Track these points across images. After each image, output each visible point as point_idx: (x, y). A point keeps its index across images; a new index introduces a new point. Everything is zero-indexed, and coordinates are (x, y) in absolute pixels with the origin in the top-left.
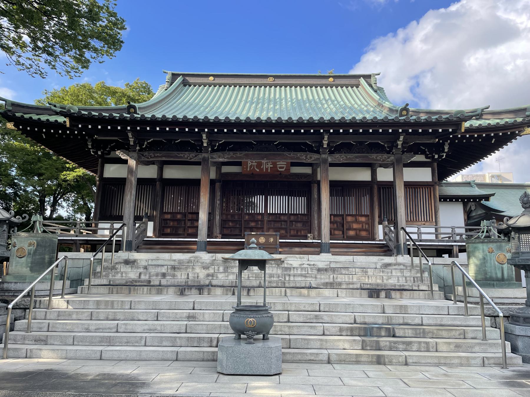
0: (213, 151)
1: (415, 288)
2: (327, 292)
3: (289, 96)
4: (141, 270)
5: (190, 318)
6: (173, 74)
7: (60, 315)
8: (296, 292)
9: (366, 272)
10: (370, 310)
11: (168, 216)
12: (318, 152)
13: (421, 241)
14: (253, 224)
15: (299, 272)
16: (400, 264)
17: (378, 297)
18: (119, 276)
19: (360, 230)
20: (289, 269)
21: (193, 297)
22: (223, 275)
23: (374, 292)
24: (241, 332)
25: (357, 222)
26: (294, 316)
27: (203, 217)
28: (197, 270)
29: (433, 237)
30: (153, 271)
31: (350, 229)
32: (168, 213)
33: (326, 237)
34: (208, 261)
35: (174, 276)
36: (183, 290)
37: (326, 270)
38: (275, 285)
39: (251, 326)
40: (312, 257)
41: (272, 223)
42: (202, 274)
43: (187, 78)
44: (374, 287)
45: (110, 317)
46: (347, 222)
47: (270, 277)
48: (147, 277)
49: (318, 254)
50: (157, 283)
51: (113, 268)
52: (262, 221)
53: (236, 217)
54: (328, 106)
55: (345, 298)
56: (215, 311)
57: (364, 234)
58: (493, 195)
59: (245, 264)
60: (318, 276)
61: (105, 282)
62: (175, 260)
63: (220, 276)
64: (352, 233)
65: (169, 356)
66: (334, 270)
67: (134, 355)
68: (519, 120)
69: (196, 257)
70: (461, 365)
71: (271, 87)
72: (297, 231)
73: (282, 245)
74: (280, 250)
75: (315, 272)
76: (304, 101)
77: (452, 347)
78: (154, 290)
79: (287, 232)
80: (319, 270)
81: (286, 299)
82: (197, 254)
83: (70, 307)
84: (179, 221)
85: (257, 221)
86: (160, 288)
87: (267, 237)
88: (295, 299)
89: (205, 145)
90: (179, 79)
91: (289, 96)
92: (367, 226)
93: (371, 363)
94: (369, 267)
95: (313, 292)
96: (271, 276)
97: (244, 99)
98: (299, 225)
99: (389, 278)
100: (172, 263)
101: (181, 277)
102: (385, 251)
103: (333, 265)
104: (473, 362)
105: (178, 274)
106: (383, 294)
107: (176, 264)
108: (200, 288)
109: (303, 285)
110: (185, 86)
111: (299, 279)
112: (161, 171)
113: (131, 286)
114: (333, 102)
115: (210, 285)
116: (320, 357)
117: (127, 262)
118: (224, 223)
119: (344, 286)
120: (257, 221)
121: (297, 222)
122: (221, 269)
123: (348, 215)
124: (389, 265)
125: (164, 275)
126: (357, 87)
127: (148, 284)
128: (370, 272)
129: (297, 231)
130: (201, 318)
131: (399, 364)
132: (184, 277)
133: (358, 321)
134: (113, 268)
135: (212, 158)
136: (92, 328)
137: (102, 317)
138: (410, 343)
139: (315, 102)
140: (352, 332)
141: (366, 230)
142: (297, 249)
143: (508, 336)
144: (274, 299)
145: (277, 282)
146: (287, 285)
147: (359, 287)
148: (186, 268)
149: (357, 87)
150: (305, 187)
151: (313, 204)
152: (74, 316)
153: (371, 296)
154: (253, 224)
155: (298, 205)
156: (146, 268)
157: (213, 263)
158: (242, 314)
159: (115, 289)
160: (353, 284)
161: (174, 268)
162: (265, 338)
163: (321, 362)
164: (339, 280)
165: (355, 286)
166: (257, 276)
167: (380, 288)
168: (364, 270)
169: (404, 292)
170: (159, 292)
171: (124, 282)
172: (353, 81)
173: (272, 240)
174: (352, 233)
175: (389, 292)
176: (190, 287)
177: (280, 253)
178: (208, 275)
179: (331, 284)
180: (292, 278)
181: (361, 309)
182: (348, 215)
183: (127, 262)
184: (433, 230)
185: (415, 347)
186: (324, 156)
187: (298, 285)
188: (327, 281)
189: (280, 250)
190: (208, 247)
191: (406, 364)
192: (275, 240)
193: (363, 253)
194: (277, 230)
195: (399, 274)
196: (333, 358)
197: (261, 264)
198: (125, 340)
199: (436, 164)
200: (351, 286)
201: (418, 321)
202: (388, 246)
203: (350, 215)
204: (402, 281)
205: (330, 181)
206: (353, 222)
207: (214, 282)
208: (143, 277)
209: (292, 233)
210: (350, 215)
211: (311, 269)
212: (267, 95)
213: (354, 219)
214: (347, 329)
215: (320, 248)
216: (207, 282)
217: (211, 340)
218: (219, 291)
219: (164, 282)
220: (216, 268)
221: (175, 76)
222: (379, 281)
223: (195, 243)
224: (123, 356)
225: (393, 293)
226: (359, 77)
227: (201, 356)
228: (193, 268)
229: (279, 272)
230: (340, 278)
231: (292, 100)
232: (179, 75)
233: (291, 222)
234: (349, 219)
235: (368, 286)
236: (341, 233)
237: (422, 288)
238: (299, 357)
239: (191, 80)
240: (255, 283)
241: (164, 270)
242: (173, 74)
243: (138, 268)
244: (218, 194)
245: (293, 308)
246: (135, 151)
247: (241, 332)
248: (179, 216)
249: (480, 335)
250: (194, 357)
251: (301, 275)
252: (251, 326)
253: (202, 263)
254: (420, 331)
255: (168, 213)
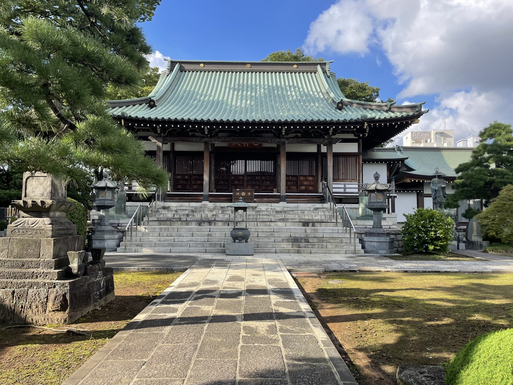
0: (211, 136)
1: (329, 221)
2: (280, 224)
3: (262, 83)
4: (174, 212)
5: (208, 235)
6: (172, 62)
7: (144, 234)
8: (262, 224)
9: (304, 213)
10: (299, 231)
11: (179, 177)
12: (279, 137)
13: (345, 193)
14: (237, 182)
15: (265, 213)
16: (324, 208)
17: (308, 226)
18: (162, 216)
19: (309, 186)
20: (260, 211)
21: (206, 227)
22: (221, 215)
23: (306, 224)
24: (235, 238)
25: (306, 180)
26: (260, 234)
27: (206, 178)
28: (206, 212)
29: (357, 190)
30: (180, 212)
31: (302, 185)
32: (179, 175)
33: (283, 191)
34: (212, 207)
35: (193, 216)
36: (200, 223)
37: (281, 212)
38: (251, 220)
39: (240, 236)
40: (273, 205)
41: (250, 181)
42: (210, 215)
43: (183, 65)
44: (307, 221)
45: (169, 235)
46: (300, 181)
47: (249, 216)
48: (178, 216)
49: (278, 202)
50: (185, 220)
51: (157, 211)
52: (243, 180)
53: (225, 177)
54: (291, 92)
55: (289, 226)
56: (221, 232)
57: (311, 188)
58: (407, 158)
59: (237, 209)
60: (276, 215)
61: (155, 219)
62: (192, 207)
63: (220, 216)
64: (303, 188)
65: (202, 251)
66: (285, 212)
67: (186, 250)
68: (411, 114)
69: (204, 205)
70: (336, 253)
71: (248, 72)
72: (267, 187)
73: (256, 197)
74: (255, 200)
75: (275, 213)
76: (273, 87)
77: (334, 246)
78: (184, 223)
79: (259, 188)
80: (277, 212)
81: (257, 227)
82: (204, 202)
83: (147, 231)
84: (186, 180)
85: (239, 180)
86: (187, 222)
87: (247, 192)
88: (262, 227)
89: (206, 133)
90: (177, 66)
91: (262, 83)
92: (313, 183)
93: (295, 253)
94: (307, 209)
95: (272, 224)
96: (249, 215)
97: (228, 85)
98: (268, 183)
99: (316, 216)
100: (191, 208)
101: (198, 216)
102: (321, 200)
103: (285, 209)
104: (341, 252)
105: (196, 214)
106: (311, 224)
107: (193, 209)
108: (210, 222)
109: (267, 220)
110: (182, 71)
111: (265, 217)
112: (173, 145)
113: (170, 221)
114: (295, 87)
115: (215, 221)
116: (272, 251)
117: (164, 208)
118: (217, 182)
119: (290, 221)
120: (239, 180)
121: (266, 180)
122: (220, 212)
123: (300, 176)
124: (318, 208)
125: (188, 215)
126: (315, 73)
127: (180, 220)
128: (306, 213)
129: (267, 187)
130: (214, 235)
131: (308, 253)
132: (199, 216)
133: (292, 236)
134: (157, 211)
135: (211, 141)
136: (162, 240)
137: (165, 235)
138: (314, 245)
139: (282, 88)
140: (288, 240)
141: (312, 186)
142: (266, 199)
143: (361, 241)
144: (251, 227)
145: (253, 219)
146: (258, 220)
147: (298, 220)
148: (200, 211)
149: (315, 73)
150: (271, 155)
151: (277, 167)
152: (151, 235)
153: (304, 226)
154: (237, 182)
155: (268, 166)
156: (176, 211)
157: (215, 208)
158: (236, 231)
159: (162, 223)
160: (295, 219)
161: (193, 211)
162: (246, 242)
163: (272, 253)
164: (288, 217)
165: (296, 221)
166: (241, 216)
167: (310, 221)
168: (303, 211)
169: (322, 223)
170: (187, 224)
171: (166, 219)
172: (312, 68)
173: (249, 194)
174: (303, 188)
175: (314, 223)
176: (204, 222)
177: (255, 202)
178: (213, 215)
179: (283, 219)
180: (261, 217)
181: (295, 231)
182: (300, 176)
183: (164, 208)
184: (357, 186)
185: (316, 246)
186: (283, 140)
187: (264, 220)
188: (281, 218)
189: (255, 200)
190: (210, 198)
191: (311, 253)
192: (252, 194)
193: (317, 199)
194: (253, 186)
195: (323, 214)
196: (278, 251)
197: (245, 209)
198: (180, 245)
199: (361, 140)
200: (294, 221)
201: (321, 236)
202: (323, 197)
203: (302, 176)
204: (323, 218)
205: (287, 153)
206: (304, 181)
207: (217, 219)
208: (176, 216)
209: (263, 188)
210: (302, 176)
211: (273, 211)
212: (245, 82)
213: (305, 178)
214: (286, 239)
215: (279, 199)
216: (213, 219)
217: (221, 244)
218: (220, 224)
219: (188, 219)
220: (217, 211)
221: (173, 64)
222: (310, 218)
223: (202, 195)
224: (180, 251)
225: (316, 224)
226: (317, 64)
227: (217, 250)
228: (204, 212)
229: (254, 213)
230: (288, 216)
231: (264, 86)
232: (176, 62)
233: (263, 180)
234: (302, 178)
235: (304, 221)
236: (296, 187)
237: (332, 221)
238: (262, 251)
239: (186, 67)
240: (240, 220)
241: (187, 212)
242: (172, 62)
243: (172, 211)
244: (213, 162)
245: (260, 231)
246: (160, 137)
247: (235, 238)
248: (186, 177)
249: (349, 241)
250: (213, 251)
251: (266, 215)
252: (240, 236)
253: (208, 208)
254: (321, 240)
255: (179, 175)
